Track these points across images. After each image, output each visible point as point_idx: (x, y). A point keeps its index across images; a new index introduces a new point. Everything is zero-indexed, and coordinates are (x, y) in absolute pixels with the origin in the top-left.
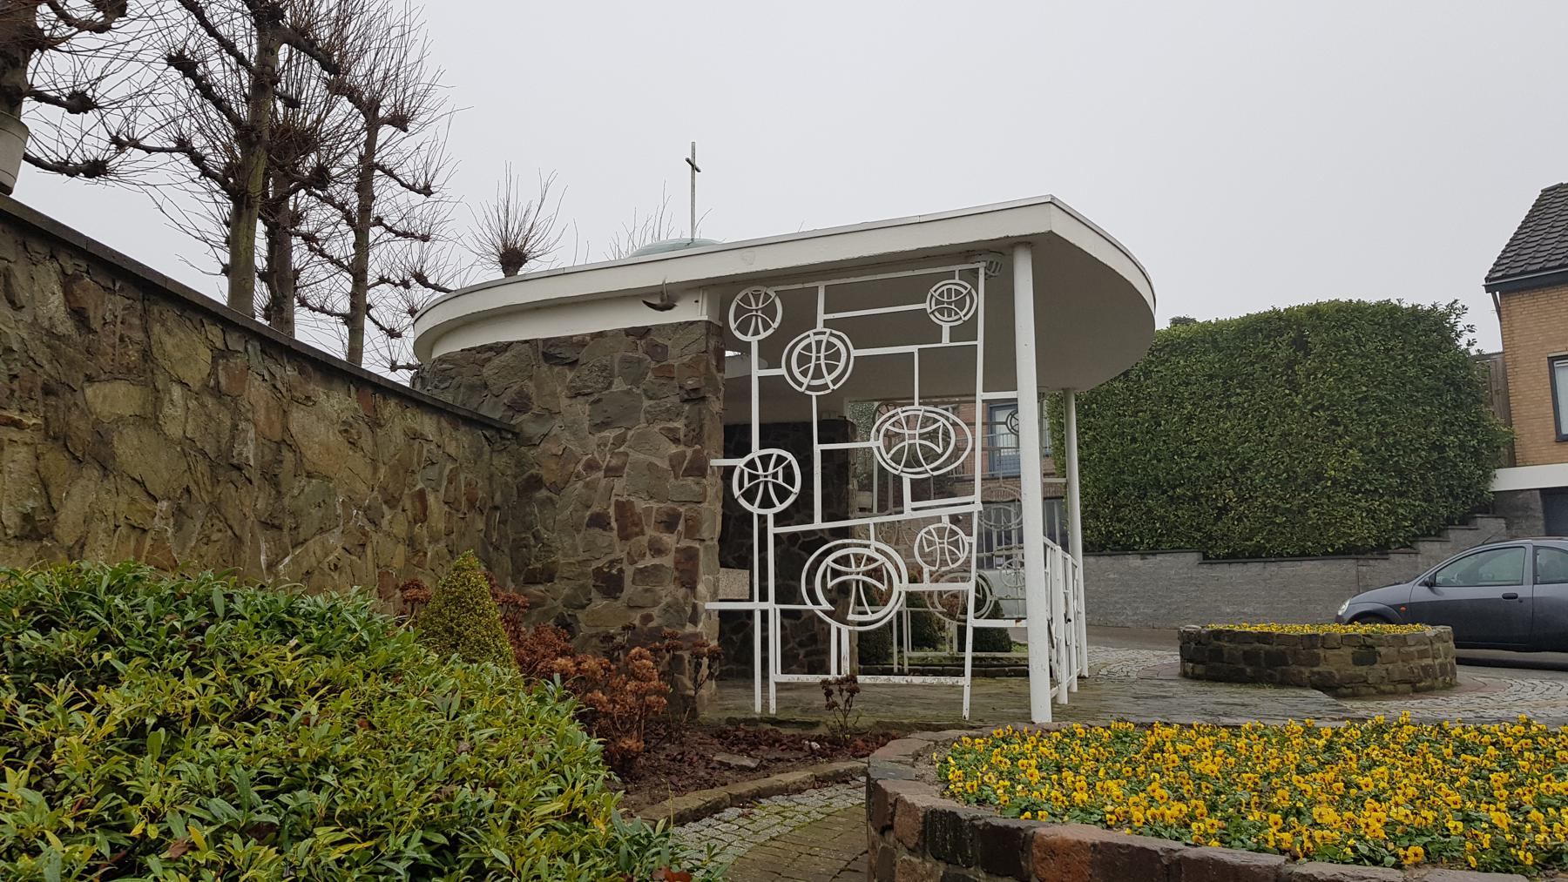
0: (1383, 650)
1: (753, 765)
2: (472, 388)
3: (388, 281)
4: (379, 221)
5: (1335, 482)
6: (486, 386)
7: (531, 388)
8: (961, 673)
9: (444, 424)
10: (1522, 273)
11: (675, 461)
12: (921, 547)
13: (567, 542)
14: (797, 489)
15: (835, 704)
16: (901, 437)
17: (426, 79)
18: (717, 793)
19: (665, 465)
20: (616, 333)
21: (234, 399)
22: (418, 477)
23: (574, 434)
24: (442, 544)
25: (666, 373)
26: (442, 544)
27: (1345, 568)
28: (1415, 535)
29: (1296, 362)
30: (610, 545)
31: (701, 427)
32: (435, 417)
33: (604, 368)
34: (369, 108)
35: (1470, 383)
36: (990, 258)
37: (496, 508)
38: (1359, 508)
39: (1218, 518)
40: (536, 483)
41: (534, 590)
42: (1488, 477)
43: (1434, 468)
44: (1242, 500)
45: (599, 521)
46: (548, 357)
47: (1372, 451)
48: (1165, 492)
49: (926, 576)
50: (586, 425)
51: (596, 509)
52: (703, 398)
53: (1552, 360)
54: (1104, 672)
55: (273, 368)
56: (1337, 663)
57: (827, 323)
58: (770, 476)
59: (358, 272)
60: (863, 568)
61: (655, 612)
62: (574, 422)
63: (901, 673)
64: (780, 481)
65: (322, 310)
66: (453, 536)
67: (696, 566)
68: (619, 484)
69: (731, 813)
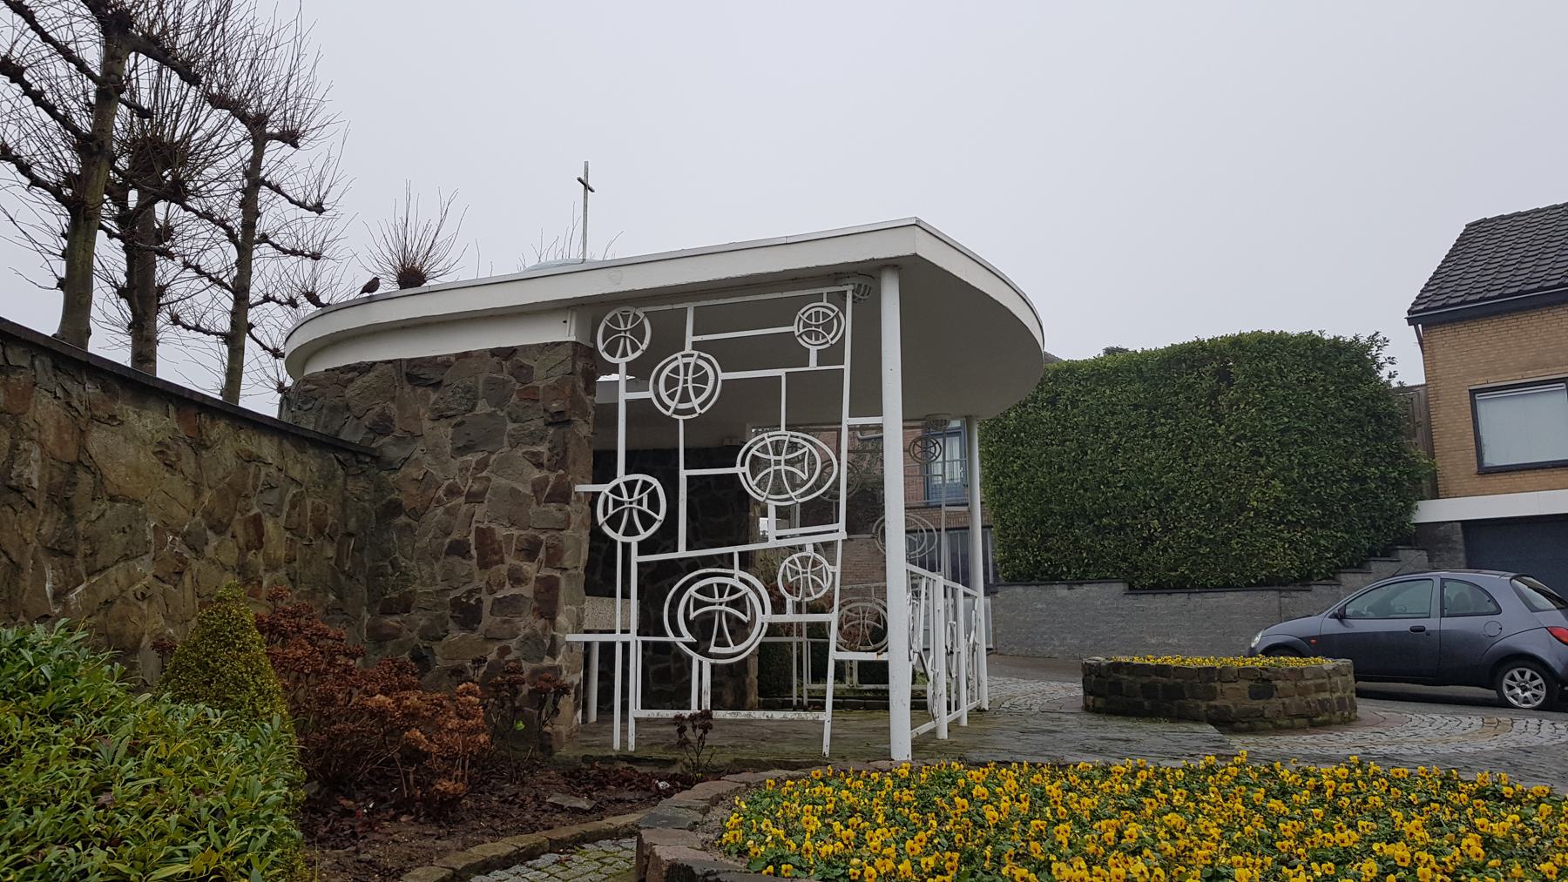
0: (1280, 684)
1: (588, 807)
2: (334, 409)
3: (274, 299)
4: (264, 238)
5: (1258, 513)
6: (348, 408)
7: (393, 409)
8: (822, 707)
9: (287, 445)
10: (1444, 306)
11: (538, 487)
12: (784, 576)
13: (426, 570)
14: (661, 517)
15: (688, 742)
16: (767, 464)
17: (318, 96)
18: (540, 837)
19: (527, 490)
20: (481, 354)
21: (15, 417)
22: (254, 501)
23: (436, 458)
24: (282, 573)
25: (531, 396)
26: (282, 573)
27: (1269, 598)
28: (1337, 567)
29: (1218, 392)
30: (470, 575)
31: (565, 451)
32: (276, 440)
33: (468, 390)
34: (257, 127)
35: (1391, 415)
36: (862, 279)
37: (350, 535)
38: (1281, 539)
39: (1144, 548)
40: (395, 508)
41: (392, 621)
42: (1409, 509)
43: (1356, 500)
44: (1166, 530)
45: (459, 549)
46: (412, 379)
47: (1294, 482)
48: (1091, 522)
49: (789, 606)
50: (449, 449)
51: (455, 536)
52: (568, 422)
53: (1473, 393)
54: (1007, 704)
55: (68, 385)
56: (1233, 697)
57: (696, 346)
58: (636, 502)
59: (240, 291)
60: (726, 598)
61: (513, 644)
62: (436, 445)
63: (800, 707)
64: (645, 507)
65: (197, 328)
66: (296, 564)
67: (556, 596)
68: (480, 510)
69: (549, 858)
